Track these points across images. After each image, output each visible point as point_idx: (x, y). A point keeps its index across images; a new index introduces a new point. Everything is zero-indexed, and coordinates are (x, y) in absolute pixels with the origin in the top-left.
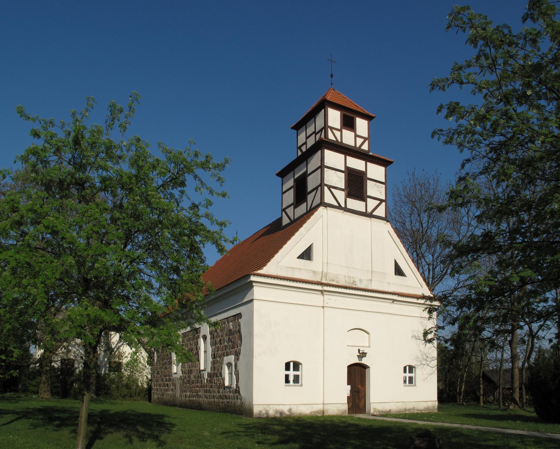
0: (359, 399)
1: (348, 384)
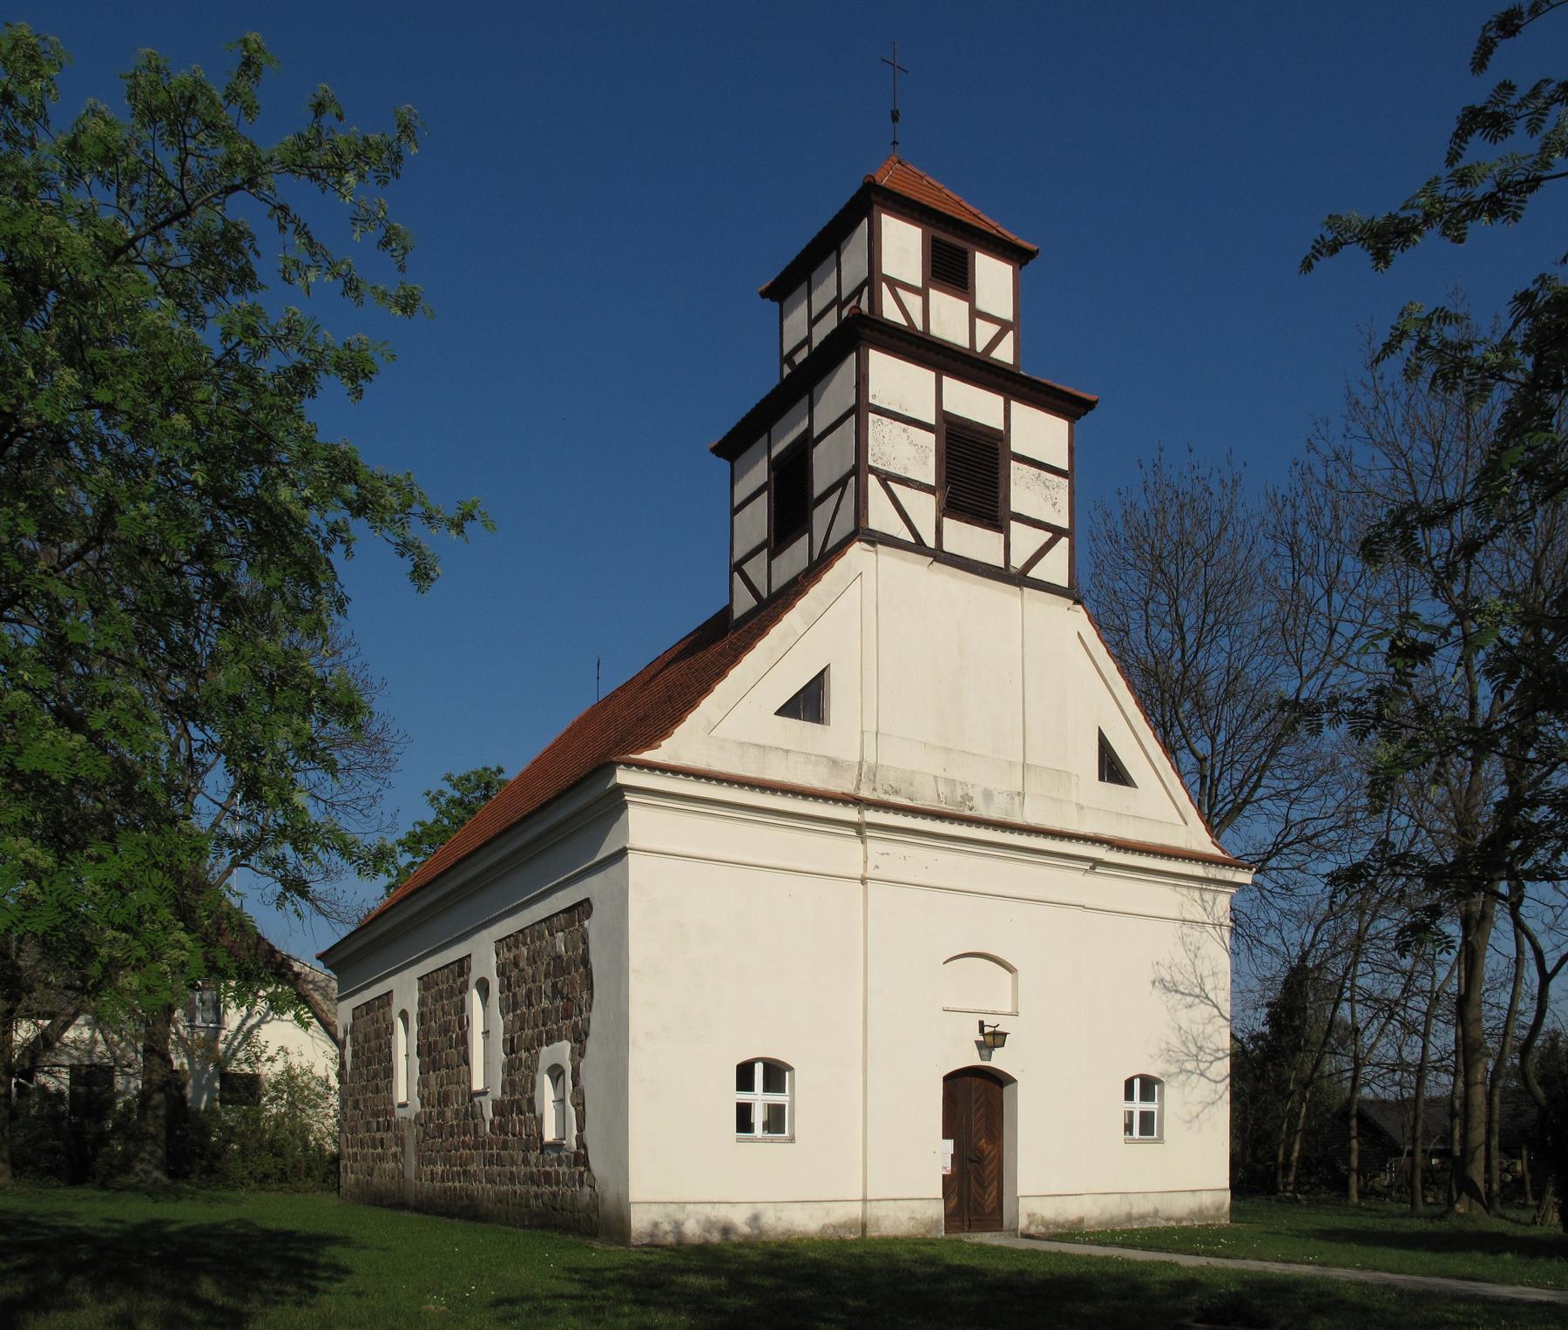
0: (981, 1183)
1: (946, 1136)
